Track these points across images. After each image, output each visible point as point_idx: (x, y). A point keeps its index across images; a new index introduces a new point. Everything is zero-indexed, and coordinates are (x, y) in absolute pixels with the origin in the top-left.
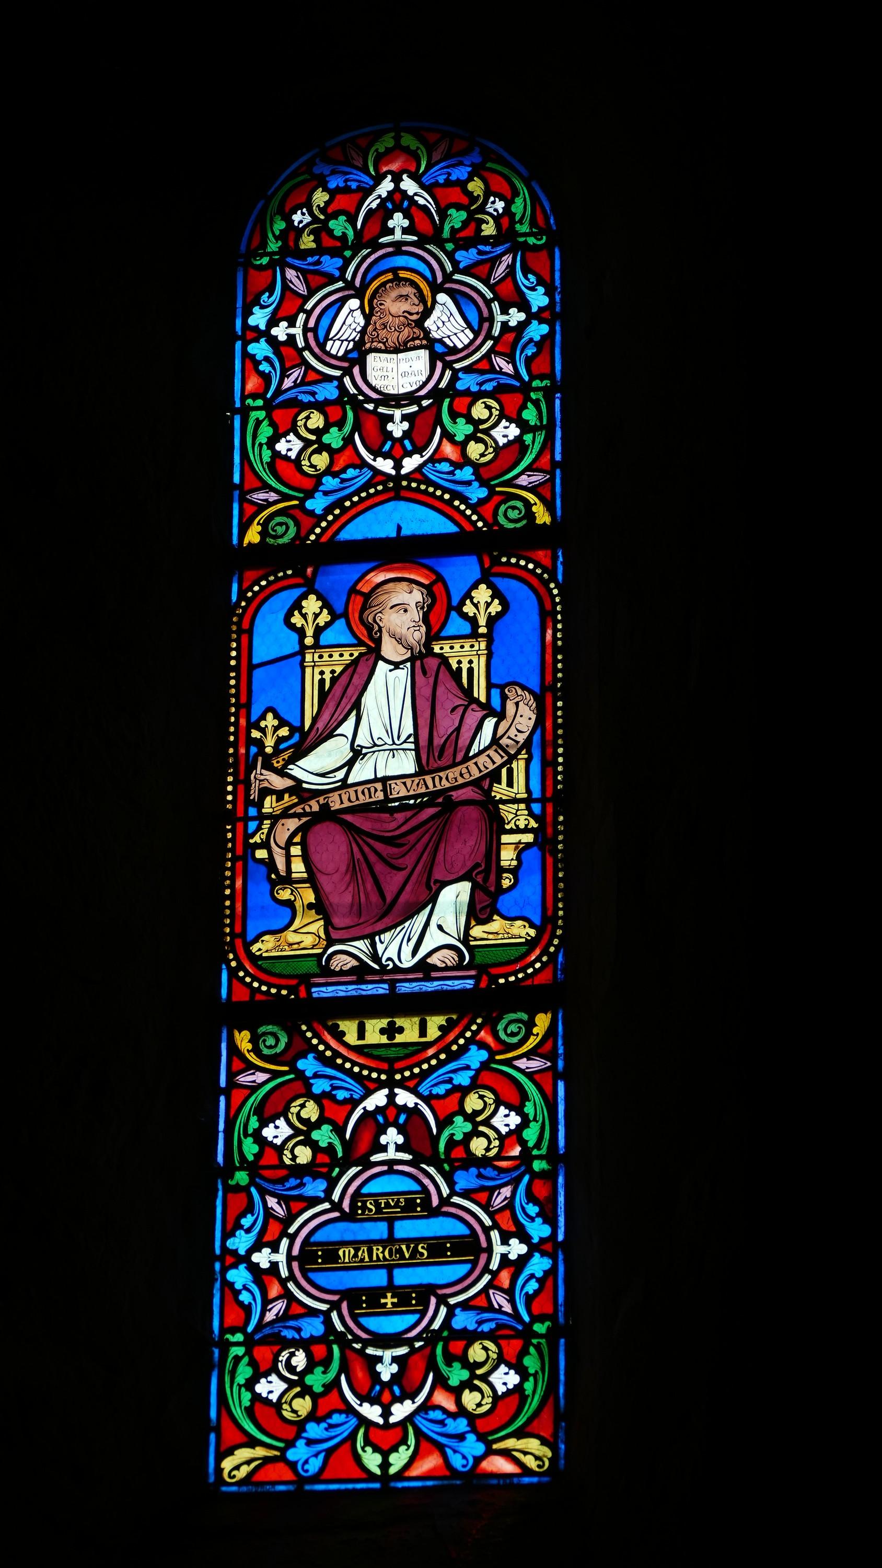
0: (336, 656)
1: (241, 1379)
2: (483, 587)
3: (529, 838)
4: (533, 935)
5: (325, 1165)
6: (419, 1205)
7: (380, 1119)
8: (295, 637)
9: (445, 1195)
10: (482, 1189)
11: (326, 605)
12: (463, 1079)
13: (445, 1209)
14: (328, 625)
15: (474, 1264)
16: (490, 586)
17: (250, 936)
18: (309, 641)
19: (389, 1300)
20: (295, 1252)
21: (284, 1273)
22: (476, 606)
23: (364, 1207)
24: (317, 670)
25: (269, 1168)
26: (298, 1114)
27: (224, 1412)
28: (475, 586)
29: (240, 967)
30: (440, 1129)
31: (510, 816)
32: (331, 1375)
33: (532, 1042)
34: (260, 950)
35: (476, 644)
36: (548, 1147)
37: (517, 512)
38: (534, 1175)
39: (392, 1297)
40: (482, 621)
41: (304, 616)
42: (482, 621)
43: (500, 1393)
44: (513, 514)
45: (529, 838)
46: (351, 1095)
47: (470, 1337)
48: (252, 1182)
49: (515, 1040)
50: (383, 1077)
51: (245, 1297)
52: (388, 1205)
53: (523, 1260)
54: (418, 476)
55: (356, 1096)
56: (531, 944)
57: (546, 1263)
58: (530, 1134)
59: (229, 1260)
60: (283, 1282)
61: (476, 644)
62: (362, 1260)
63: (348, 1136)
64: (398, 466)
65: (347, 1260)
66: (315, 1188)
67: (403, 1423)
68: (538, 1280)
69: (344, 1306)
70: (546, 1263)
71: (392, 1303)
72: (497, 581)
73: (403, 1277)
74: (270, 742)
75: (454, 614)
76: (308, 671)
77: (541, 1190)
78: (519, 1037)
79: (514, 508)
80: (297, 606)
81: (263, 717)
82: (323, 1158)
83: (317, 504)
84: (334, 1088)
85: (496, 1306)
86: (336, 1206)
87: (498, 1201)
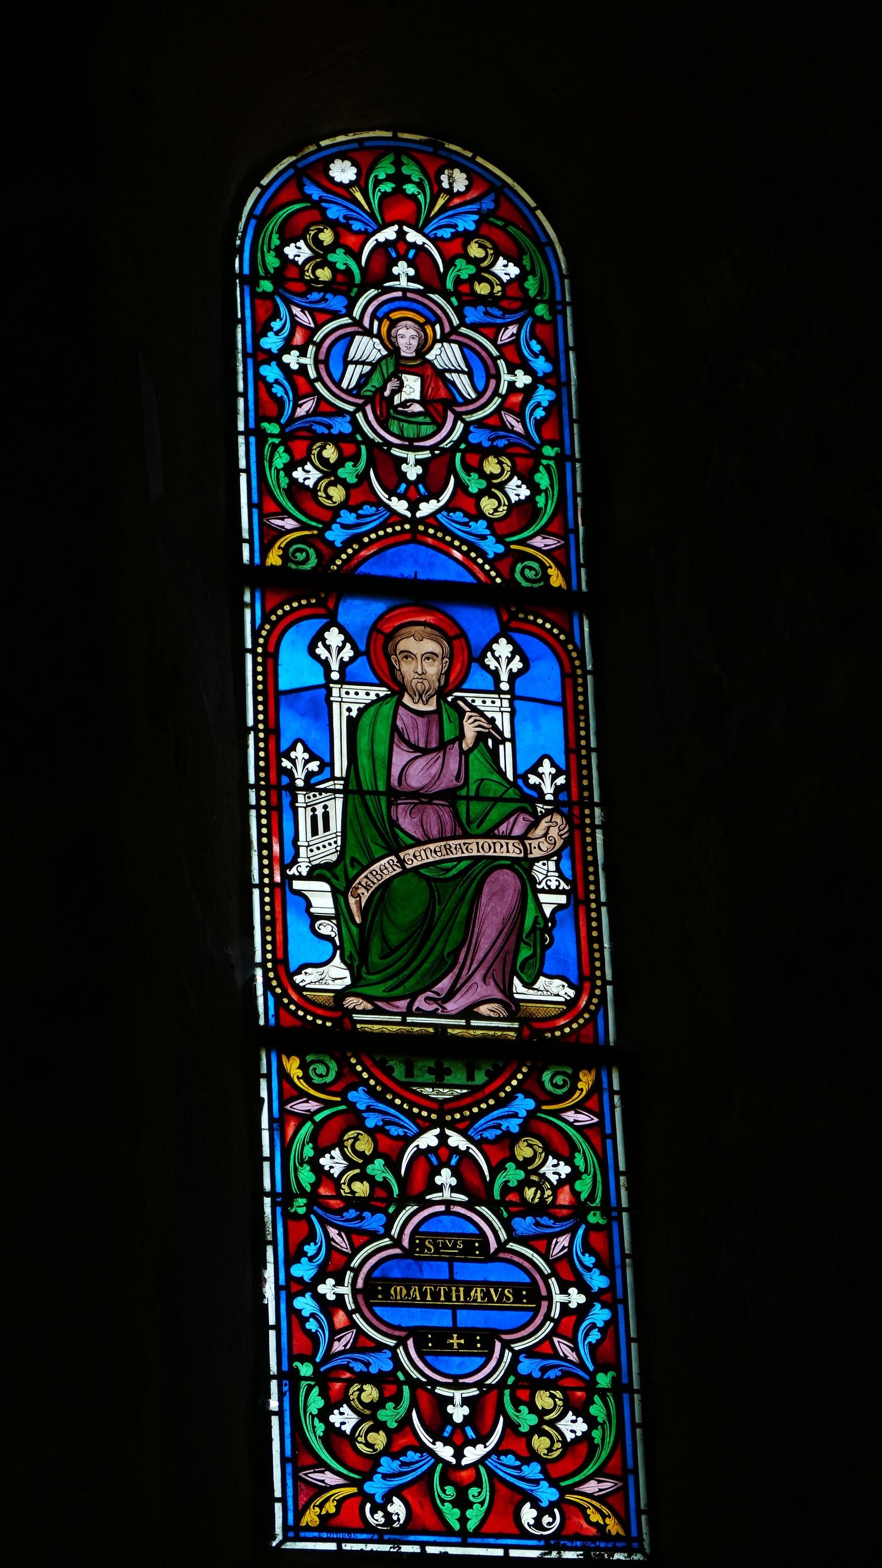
0: (362, 694)
1: (587, 1179)
2: (503, 641)
3: (562, 899)
4: (573, 996)
5: (380, 1200)
6: (477, 1249)
7: (434, 1159)
8: (320, 669)
9: (401, 1348)
10: (364, 1350)
11: (348, 639)
12: (513, 1125)
13: (501, 1255)
14: (352, 660)
15: (536, 1311)
16: (510, 641)
17: (293, 966)
18: (335, 676)
19: (455, 1341)
20: (545, 1304)
21: (350, 1306)
22: (497, 659)
23: (422, 1246)
24: (345, 706)
25: (325, 1199)
26: (500, 505)
27: (600, 1151)
28: (495, 640)
29: (285, 994)
30: (494, 1175)
31: (541, 877)
32: (402, 1410)
33: (577, 1097)
34: (303, 981)
35: (498, 702)
36: (602, 1201)
37: (533, 572)
38: (590, 1228)
39: (458, 1338)
40: (504, 676)
41: (328, 648)
42: (504, 676)
43: (569, 1440)
44: (530, 574)
45: (562, 899)
46: (499, 1459)
47: (534, 1384)
48: (593, 1375)
49: (559, 1092)
50: (434, 1116)
51: (312, 1325)
52: (445, 1246)
53: (583, 1310)
54: (432, 521)
55: (410, 1134)
56: (571, 1003)
57: (605, 1314)
58: (583, 1186)
59: (607, 1297)
60: (349, 1314)
61: (498, 702)
62: (414, 1299)
63: (501, 1419)
64: (443, 1138)
65: (398, 1297)
66: (375, 1222)
67: (475, 1465)
68: (600, 1330)
69: (410, 1343)
70: (605, 1314)
71: (458, 1344)
72: (517, 636)
73: (467, 1319)
74: (300, 775)
75: (475, 665)
76: (336, 706)
77: (597, 1240)
78: (565, 1090)
79: (531, 568)
80: (319, 637)
81: (293, 748)
82: (523, 1394)
83: (336, 535)
84: (518, 1468)
85: (562, 1354)
86: (506, 1345)
87: (349, 1337)
